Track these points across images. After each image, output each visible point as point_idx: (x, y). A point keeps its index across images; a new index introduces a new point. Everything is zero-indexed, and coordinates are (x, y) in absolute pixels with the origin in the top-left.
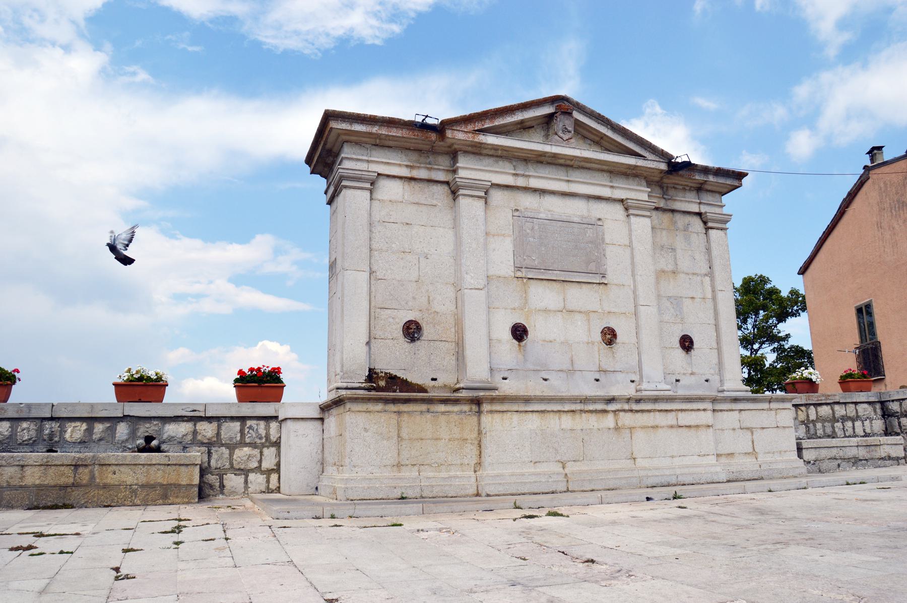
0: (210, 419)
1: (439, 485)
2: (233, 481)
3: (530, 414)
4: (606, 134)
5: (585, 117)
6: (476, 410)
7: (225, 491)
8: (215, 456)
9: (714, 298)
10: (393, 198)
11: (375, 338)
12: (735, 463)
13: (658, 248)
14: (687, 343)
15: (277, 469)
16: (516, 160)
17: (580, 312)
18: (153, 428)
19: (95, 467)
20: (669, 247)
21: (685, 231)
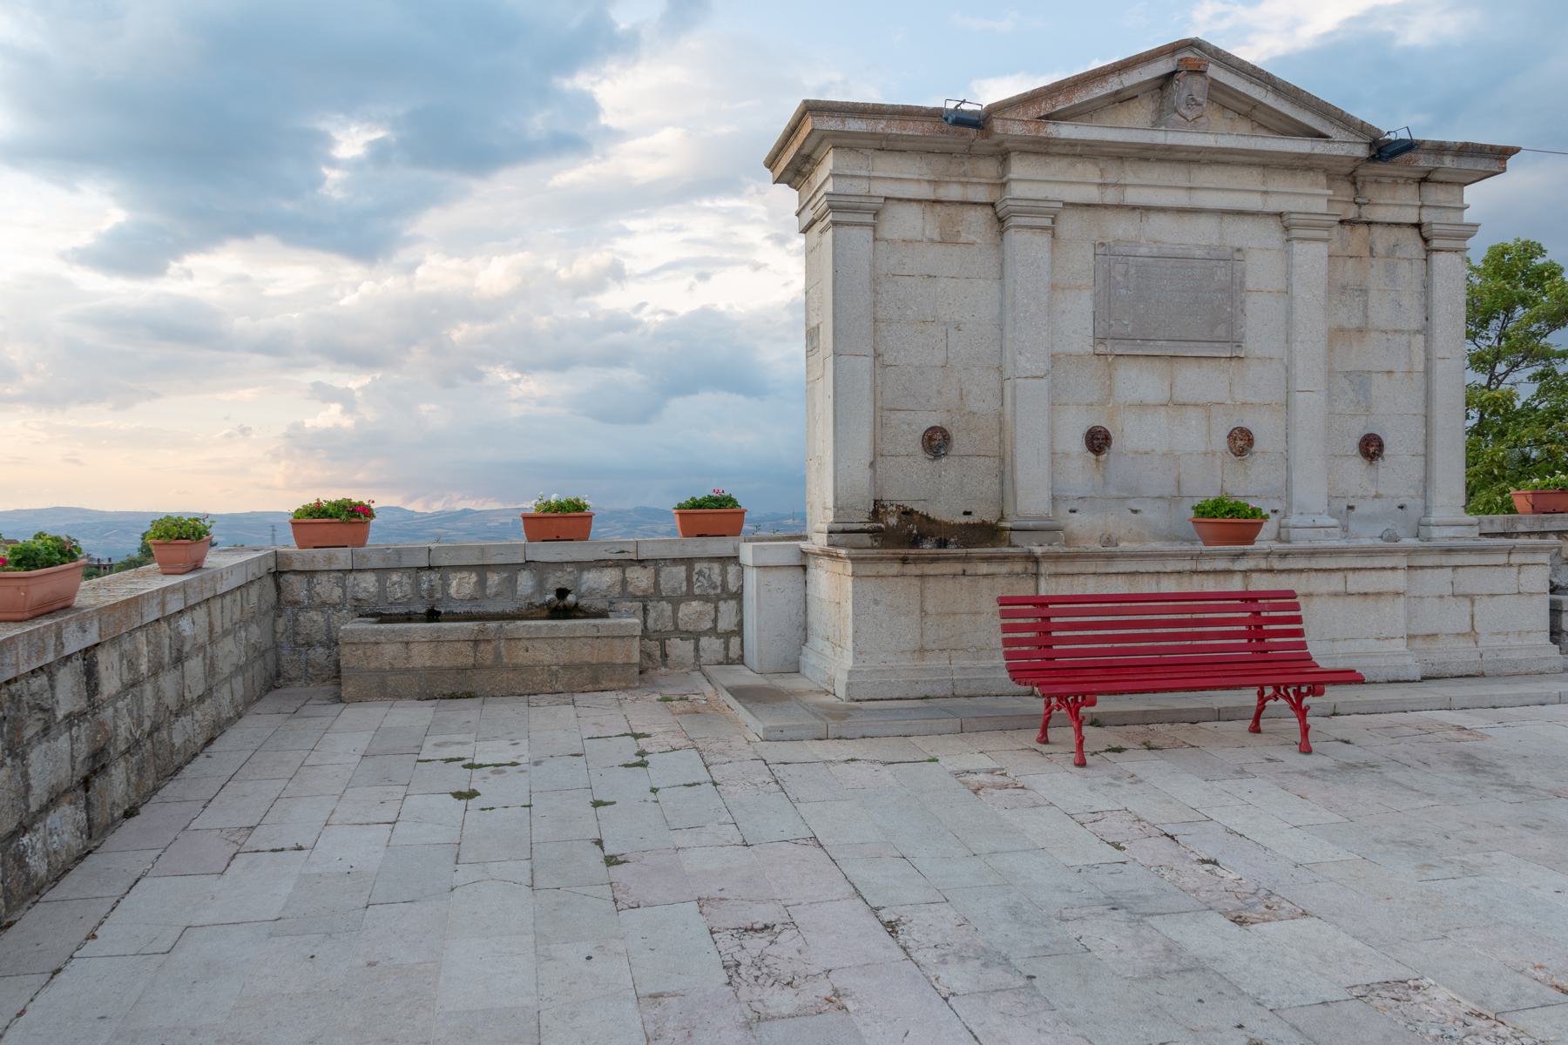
0: (641, 562)
1: (979, 679)
2: (680, 649)
3: (1114, 577)
4: (1264, 101)
5: (1229, 74)
6: (1033, 572)
7: (669, 662)
8: (652, 615)
9: (1428, 372)
10: (909, 235)
11: (882, 455)
12: (1439, 649)
13: (1337, 290)
14: (1371, 448)
15: (739, 631)
16: (1105, 158)
17: (1196, 405)
18: (567, 577)
19: (500, 643)
20: (1355, 287)
21: (1388, 257)
